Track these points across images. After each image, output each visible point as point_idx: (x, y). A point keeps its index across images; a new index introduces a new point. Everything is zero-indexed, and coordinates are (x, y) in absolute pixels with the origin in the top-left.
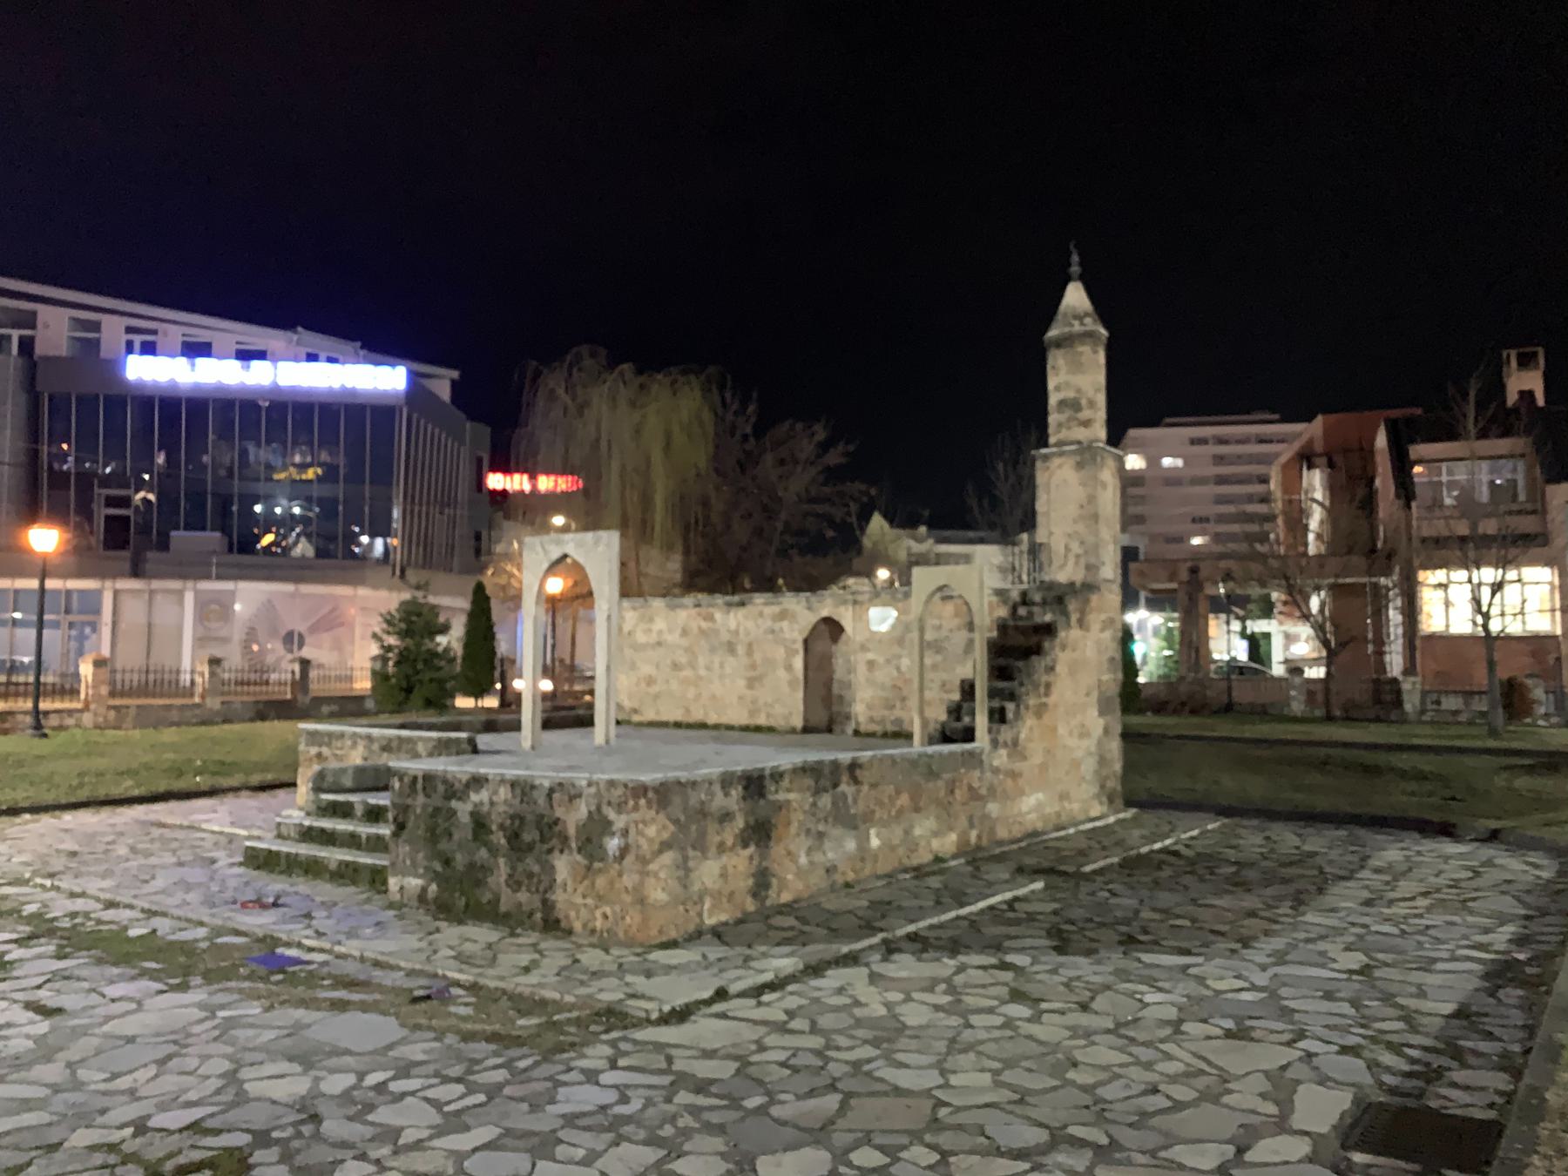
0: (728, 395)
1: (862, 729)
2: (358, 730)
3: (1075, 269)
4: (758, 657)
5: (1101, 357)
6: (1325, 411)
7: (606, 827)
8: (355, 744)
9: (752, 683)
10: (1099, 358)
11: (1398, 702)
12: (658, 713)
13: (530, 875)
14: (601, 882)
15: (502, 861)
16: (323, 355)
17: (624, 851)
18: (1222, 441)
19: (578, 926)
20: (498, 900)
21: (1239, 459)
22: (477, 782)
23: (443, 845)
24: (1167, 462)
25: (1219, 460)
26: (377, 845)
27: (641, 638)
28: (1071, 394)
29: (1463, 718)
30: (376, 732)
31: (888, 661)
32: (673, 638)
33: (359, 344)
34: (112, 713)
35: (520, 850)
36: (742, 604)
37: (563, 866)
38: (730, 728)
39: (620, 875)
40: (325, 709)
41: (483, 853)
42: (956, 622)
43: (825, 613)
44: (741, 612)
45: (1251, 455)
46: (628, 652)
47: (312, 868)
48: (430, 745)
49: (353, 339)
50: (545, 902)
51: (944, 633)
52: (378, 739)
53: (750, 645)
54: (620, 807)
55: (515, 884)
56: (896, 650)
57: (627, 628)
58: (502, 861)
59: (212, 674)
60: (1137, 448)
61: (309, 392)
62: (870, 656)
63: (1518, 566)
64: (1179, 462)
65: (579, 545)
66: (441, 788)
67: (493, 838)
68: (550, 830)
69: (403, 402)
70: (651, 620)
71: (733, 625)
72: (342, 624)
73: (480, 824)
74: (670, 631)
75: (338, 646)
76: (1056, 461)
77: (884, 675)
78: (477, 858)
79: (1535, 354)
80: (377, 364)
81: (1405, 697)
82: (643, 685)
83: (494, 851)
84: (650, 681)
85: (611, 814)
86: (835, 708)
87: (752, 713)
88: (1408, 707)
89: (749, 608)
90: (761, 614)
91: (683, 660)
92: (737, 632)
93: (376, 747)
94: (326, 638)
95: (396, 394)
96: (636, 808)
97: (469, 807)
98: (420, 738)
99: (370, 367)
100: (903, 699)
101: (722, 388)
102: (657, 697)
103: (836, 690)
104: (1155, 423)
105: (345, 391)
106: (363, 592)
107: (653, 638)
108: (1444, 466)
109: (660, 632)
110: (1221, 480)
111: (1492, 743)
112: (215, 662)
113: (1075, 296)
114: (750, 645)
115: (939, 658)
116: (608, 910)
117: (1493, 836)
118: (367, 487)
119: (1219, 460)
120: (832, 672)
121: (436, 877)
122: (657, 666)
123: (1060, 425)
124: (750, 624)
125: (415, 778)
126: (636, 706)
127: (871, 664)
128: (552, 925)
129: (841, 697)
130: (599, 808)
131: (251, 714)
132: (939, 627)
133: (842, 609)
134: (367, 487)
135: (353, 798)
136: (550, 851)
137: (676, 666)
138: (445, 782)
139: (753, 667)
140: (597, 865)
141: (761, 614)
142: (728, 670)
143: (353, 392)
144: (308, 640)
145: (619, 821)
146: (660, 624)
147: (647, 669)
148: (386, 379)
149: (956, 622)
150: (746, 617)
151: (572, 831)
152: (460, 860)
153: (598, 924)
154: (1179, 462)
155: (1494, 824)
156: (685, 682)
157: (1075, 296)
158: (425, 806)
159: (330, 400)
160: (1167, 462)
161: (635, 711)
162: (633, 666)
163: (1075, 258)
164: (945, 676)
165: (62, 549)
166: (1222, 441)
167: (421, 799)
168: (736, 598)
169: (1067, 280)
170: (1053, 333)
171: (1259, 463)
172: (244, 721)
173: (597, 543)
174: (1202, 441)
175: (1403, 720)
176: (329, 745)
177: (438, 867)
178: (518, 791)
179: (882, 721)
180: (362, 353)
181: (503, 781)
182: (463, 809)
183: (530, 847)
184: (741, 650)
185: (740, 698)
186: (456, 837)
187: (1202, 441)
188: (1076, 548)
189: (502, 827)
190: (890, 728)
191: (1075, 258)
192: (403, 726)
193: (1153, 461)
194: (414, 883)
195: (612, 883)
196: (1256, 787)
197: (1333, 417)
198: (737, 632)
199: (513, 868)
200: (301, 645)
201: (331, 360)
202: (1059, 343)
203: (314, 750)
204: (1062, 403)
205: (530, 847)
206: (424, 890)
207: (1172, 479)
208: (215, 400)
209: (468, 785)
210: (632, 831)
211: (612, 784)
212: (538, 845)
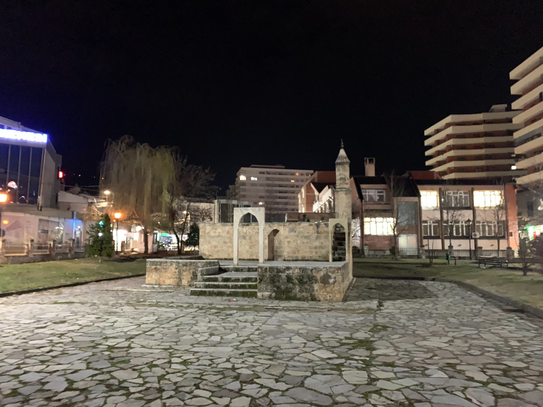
0: (178, 156)
1: (286, 259)
2: (173, 260)
3: (343, 146)
4: (253, 240)
5: (348, 168)
6: (318, 170)
7: (330, 277)
8: (171, 265)
9: (250, 248)
10: (347, 167)
11: (363, 253)
12: (218, 256)
13: (306, 289)
14: (328, 289)
15: (297, 286)
16: (6, 126)
17: (334, 282)
18: (268, 173)
19: (322, 299)
20: (296, 295)
21: (273, 179)
22: (288, 268)
23: (277, 284)
24: (252, 179)
25: (268, 179)
26: (255, 287)
27: (212, 234)
28: (344, 177)
29: (378, 257)
30: (180, 261)
31: (294, 241)
32: (224, 234)
33: (20, 123)
34: (6, 259)
35: (302, 283)
36: (248, 225)
37: (316, 287)
38: (245, 260)
39: (334, 287)
40: (59, 257)
41: (291, 285)
42: (313, 231)
43: (275, 228)
44: (247, 228)
45: (276, 178)
46: (208, 238)
47: (211, 294)
48: (203, 264)
49: (18, 121)
50: (311, 294)
51: (310, 234)
52: (181, 263)
53: (250, 237)
54: (333, 273)
55: (301, 291)
56: (297, 238)
57: (207, 231)
58: (297, 286)
59: (32, 245)
60: (244, 173)
61: (8, 140)
62: (288, 240)
63: (375, 217)
64: (256, 179)
65: (253, 211)
66: (276, 271)
67: (294, 281)
68: (312, 279)
69: (45, 147)
70: (216, 229)
71: (245, 231)
72: (20, 227)
73: (289, 279)
74: (223, 232)
75: (17, 236)
76: (340, 192)
77: (293, 245)
78: (289, 286)
79: (373, 160)
80: (27, 131)
81: (365, 251)
82: (213, 248)
83: (294, 284)
84: (215, 247)
85: (330, 274)
86: (275, 254)
87: (251, 255)
88: (366, 254)
89: (250, 226)
90: (254, 228)
91: (228, 241)
92: (246, 233)
93: (181, 265)
94: (13, 232)
95: (43, 144)
96: (338, 273)
97: (286, 274)
98: (199, 262)
99: (33, 133)
100: (299, 251)
101: (177, 153)
102: (218, 251)
103: (275, 249)
104: (248, 166)
105: (22, 141)
106: (28, 215)
107: (217, 234)
108: (367, 190)
109: (219, 233)
110: (268, 185)
111: (397, 262)
112: (32, 241)
113: (342, 152)
114: (250, 237)
115: (309, 240)
116: (331, 295)
117: (434, 280)
118: (29, 177)
119: (268, 179)
120: (274, 244)
121: (274, 291)
122: (218, 242)
123: (341, 184)
124: (251, 231)
125: (266, 268)
126: (211, 254)
127: (289, 242)
128: (313, 299)
129: (277, 251)
130: (327, 273)
131: (40, 259)
132: (309, 233)
133: (280, 227)
134: (29, 177)
135: (217, 276)
136: (312, 283)
137: (225, 243)
138: (277, 269)
139: (251, 243)
140: (327, 285)
141: (254, 228)
142: (243, 244)
143: (26, 142)
144: (6, 233)
145: (333, 276)
146: (219, 230)
147: (214, 243)
148: (41, 139)
149: (313, 231)
150: (249, 229)
151: (319, 278)
152: (283, 287)
153: (328, 298)
154: (256, 179)
155: (433, 277)
156: (229, 247)
157: (342, 152)
158: (270, 275)
159: (16, 144)
160: (252, 179)
161: (210, 256)
162: (209, 243)
163: (342, 143)
164: (311, 245)
165: (9, 200)
166: (268, 173)
167: (268, 273)
168: (246, 224)
169: (341, 148)
170: (338, 161)
171: (279, 181)
172: (39, 262)
173: (259, 210)
174: (263, 173)
175: (365, 257)
176: (160, 265)
177: (275, 289)
178: (301, 270)
179: (292, 257)
180: (21, 126)
181: (297, 268)
182: (283, 275)
183: (306, 283)
184: (247, 238)
185: (247, 251)
186: (281, 281)
187: (263, 173)
188: (345, 214)
189: (296, 278)
190: (295, 259)
191: (342, 143)
192: (191, 259)
193: (248, 178)
194: (267, 294)
195: (332, 289)
196: (372, 273)
197: (321, 172)
198: (246, 233)
199: (301, 288)
200: (4, 234)
201: (9, 128)
202: (340, 164)
203: (153, 267)
204: (341, 179)
205: (306, 283)
206: (271, 295)
207: (254, 184)
208: (33, 148)
209: (285, 269)
210: (337, 277)
211: (331, 267)
212: (308, 282)
